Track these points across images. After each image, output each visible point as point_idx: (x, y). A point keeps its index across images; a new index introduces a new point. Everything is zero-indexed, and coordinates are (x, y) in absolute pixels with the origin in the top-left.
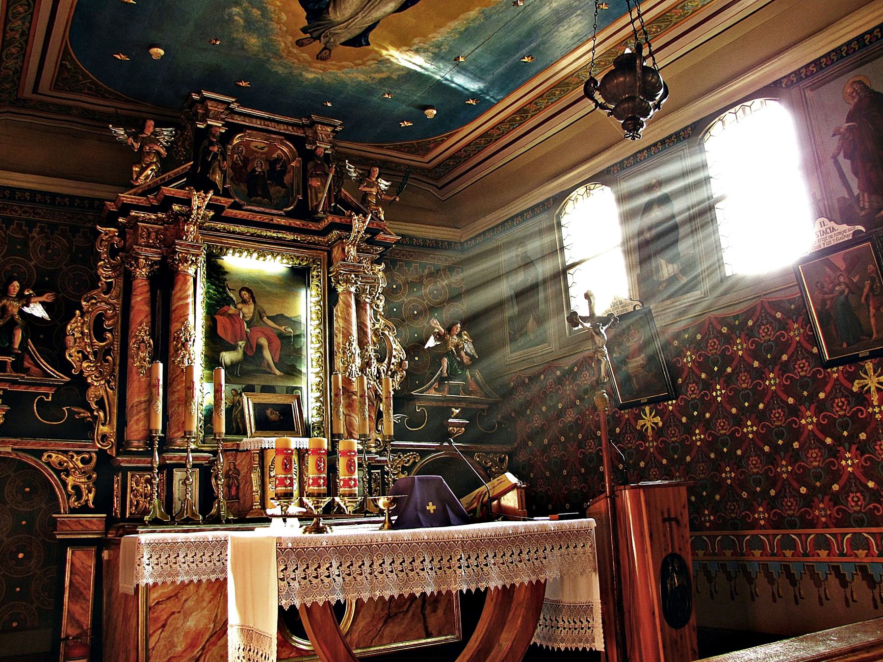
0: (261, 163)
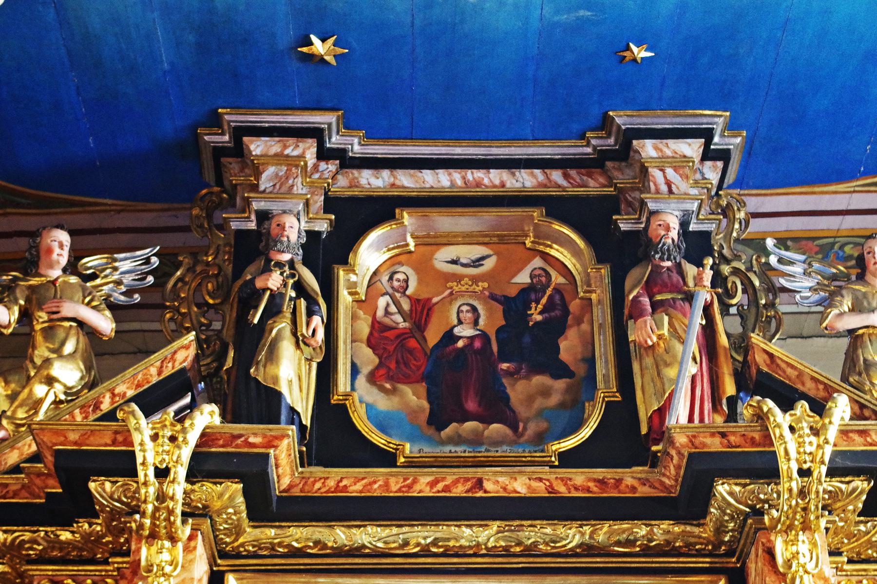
0: (474, 309)
